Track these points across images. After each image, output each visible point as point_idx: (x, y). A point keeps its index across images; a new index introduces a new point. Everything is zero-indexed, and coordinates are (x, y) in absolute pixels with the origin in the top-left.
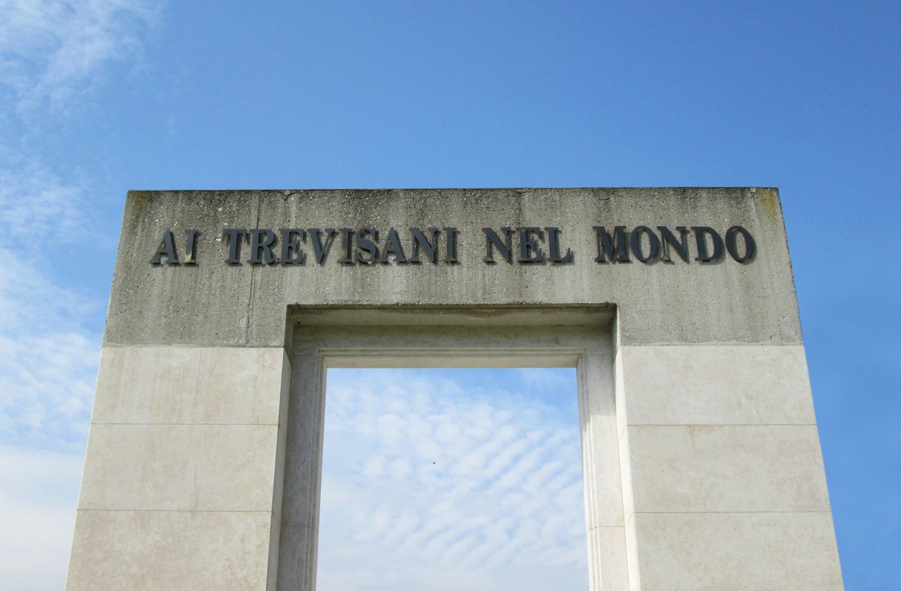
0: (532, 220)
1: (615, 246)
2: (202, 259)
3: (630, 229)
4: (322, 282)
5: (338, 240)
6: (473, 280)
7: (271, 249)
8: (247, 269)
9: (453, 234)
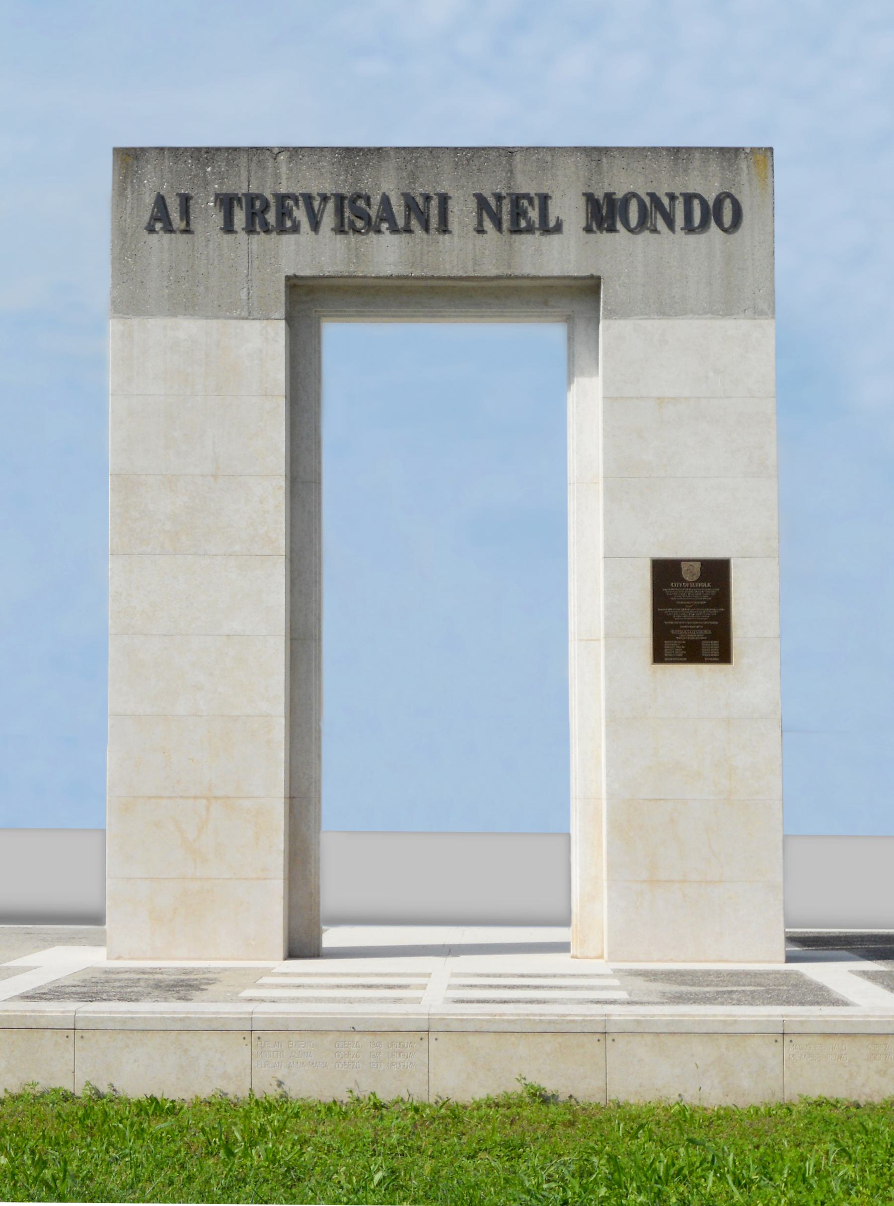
0: (526, 185)
1: (604, 214)
2: (197, 224)
3: (620, 195)
4: (316, 251)
5: (331, 205)
6: (467, 250)
7: (264, 214)
8: (242, 236)
9: (444, 199)
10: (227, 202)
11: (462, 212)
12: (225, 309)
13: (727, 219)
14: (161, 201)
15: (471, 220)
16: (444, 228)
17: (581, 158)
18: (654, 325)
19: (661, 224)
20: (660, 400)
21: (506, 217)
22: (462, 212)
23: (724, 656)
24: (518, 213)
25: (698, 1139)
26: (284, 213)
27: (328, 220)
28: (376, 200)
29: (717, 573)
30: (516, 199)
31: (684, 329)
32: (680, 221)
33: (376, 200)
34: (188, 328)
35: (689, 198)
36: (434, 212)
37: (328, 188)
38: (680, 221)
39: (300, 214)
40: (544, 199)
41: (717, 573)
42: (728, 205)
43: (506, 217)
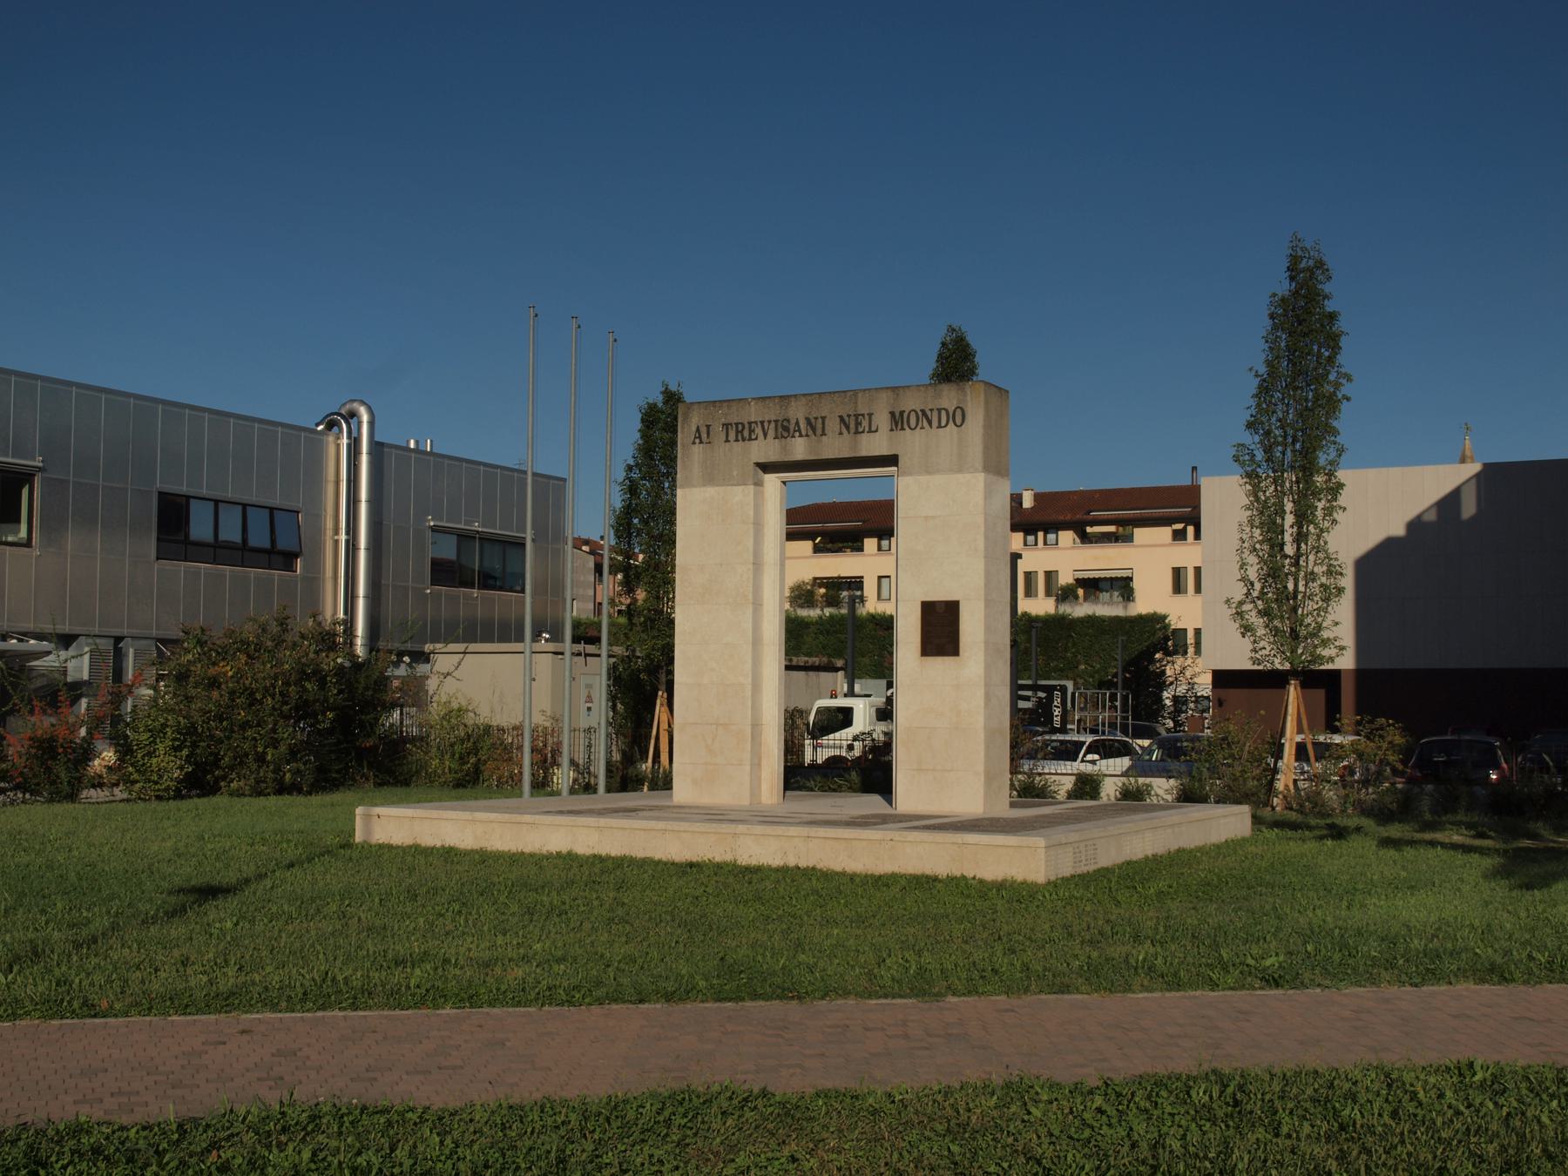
0: (862, 410)
10: (726, 426)
11: (833, 425)
12: (727, 481)
13: (958, 421)
14: (698, 430)
15: (837, 428)
16: (824, 434)
17: (890, 393)
18: (924, 479)
19: (925, 424)
20: (926, 518)
21: (852, 426)
22: (833, 425)
23: (955, 651)
24: (858, 424)
25: (1329, 843)
26: (751, 431)
27: (771, 433)
28: (793, 422)
29: (952, 608)
30: (857, 416)
31: (938, 479)
32: (935, 423)
33: (793, 422)
34: (711, 492)
35: (939, 410)
36: (819, 426)
37: (773, 418)
38: (935, 423)
39: (759, 431)
40: (870, 415)
41: (952, 608)
42: (959, 412)
43: (852, 426)
